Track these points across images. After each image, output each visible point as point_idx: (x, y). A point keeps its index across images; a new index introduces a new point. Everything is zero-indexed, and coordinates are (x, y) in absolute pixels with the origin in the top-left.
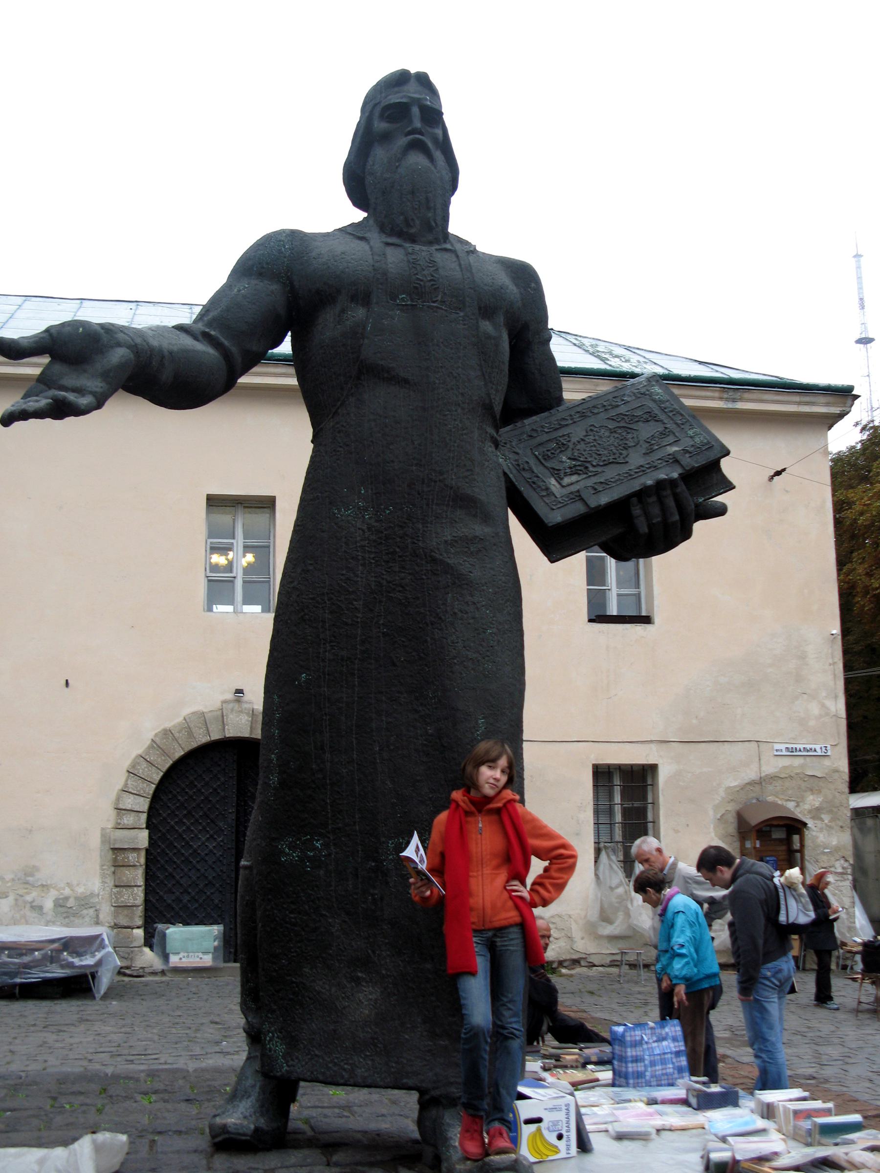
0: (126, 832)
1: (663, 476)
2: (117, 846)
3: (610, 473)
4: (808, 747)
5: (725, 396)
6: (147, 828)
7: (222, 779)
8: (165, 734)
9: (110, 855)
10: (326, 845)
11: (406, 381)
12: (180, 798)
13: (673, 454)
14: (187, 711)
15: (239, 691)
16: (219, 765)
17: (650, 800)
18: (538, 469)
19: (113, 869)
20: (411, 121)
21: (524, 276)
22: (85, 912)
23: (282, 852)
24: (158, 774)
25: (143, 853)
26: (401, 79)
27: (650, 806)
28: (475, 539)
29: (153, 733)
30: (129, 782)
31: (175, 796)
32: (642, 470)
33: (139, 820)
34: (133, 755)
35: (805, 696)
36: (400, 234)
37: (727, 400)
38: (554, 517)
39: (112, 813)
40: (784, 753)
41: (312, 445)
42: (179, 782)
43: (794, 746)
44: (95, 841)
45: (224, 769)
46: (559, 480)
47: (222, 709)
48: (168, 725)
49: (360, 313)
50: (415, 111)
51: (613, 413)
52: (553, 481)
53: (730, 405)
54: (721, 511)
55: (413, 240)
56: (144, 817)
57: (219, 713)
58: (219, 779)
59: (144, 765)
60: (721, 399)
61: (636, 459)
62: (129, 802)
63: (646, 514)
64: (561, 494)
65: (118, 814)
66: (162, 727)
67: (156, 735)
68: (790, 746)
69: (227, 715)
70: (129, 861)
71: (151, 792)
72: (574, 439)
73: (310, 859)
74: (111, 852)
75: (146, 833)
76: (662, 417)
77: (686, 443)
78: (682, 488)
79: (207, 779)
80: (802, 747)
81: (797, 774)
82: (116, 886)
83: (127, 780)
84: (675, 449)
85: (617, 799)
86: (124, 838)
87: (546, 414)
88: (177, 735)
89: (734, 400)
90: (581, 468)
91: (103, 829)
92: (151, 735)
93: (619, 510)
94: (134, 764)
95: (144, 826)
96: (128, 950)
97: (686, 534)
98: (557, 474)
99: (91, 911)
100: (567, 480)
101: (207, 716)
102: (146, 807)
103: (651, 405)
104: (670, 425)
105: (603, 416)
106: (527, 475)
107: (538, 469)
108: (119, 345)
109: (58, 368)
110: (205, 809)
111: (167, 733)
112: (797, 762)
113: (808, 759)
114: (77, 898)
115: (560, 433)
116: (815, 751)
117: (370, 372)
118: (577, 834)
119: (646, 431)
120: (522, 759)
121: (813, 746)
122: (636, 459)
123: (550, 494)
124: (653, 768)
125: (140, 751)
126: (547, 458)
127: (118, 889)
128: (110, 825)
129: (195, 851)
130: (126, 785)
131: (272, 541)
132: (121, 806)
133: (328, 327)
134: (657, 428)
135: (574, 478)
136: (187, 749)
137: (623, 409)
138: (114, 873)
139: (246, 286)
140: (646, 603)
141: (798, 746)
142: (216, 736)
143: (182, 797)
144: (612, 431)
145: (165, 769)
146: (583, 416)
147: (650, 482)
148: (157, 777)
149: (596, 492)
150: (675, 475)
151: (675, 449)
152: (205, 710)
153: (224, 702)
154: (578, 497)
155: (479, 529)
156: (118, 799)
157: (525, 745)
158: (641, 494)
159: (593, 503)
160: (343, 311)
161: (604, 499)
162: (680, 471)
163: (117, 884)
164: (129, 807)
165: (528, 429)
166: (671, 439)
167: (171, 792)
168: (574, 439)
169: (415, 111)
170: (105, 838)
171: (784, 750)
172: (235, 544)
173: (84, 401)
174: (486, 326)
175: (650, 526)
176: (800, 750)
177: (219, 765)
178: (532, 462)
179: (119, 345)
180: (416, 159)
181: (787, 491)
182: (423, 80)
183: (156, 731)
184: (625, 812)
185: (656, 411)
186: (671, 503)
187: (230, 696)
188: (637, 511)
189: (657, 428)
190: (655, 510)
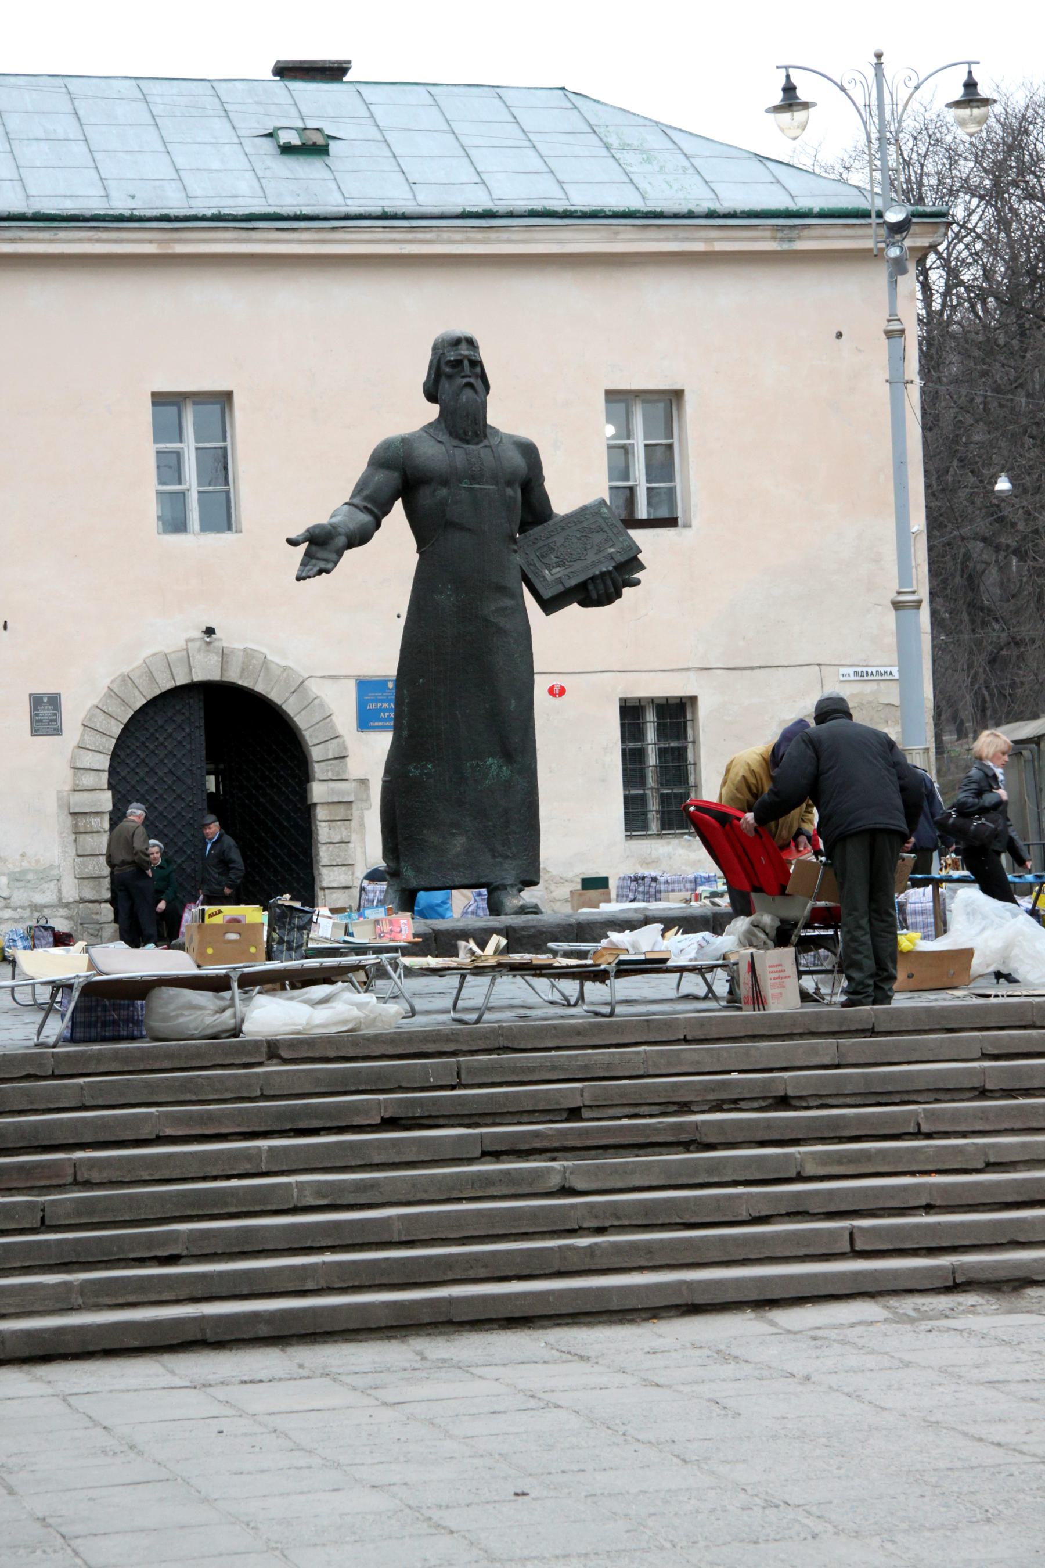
0: (85, 795)
1: (604, 569)
2: (77, 810)
3: (577, 566)
4: (882, 670)
5: (780, 235)
6: (109, 789)
7: (188, 730)
8: (124, 681)
9: (69, 821)
10: (434, 766)
11: (470, 530)
12: (139, 753)
13: (611, 554)
14: (147, 652)
15: (210, 631)
16: (183, 714)
17: (690, 738)
18: (538, 564)
19: (74, 836)
20: (463, 369)
21: (529, 451)
22: (46, 886)
23: (410, 771)
24: (118, 726)
25: (107, 818)
26: (457, 342)
27: (690, 746)
28: (506, 608)
29: (109, 680)
30: (86, 737)
31: (134, 751)
32: (594, 564)
33: (100, 779)
34: (88, 706)
35: (880, 608)
36: (461, 439)
37: (782, 239)
38: (547, 594)
39: (70, 773)
40: (852, 678)
41: (418, 556)
42: (137, 734)
43: (865, 669)
44: (51, 806)
45: (189, 719)
46: (550, 571)
47: (187, 649)
48: (125, 670)
49: (444, 492)
50: (466, 362)
51: (579, 527)
52: (547, 572)
53: (786, 246)
54: (637, 583)
55: (468, 442)
56: (106, 775)
57: (185, 653)
58: (183, 729)
59: (102, 716)
60: (774, 238)
61: (591, 557)
62: (90, 760)
63: (596, 588)
64: (552, 577)
65: (75, 775)
66: (118, 673)
67: (112, 682)
68: (859, 669)
69: (193, 656)
70: (91, 826)
71: (112, 748)
72: (558, 544)
73: (426, 774)
74: (70, 817)
75: (109, 794)
76: (606, 529)
77: (619, 546)
78: (615, 574)
79: (170, 730)
80: (874, 670)
81: (870, 703)
82: (79, 856)
83: (82, 735)
84: (612, 550)
85: (651, 735)
86: (83, 801)
87: (540, 527)
88: (136, 681)
89: (791, 240)
90: (561, 564)
91: (59, 792)
92: (106, 682)
93: (583, 586)
94: (90, 716)
95: (106, 786)
96: (98, 926)
97: (619, 595)
98: (548, 567)
99: (52, 885)
100: (554, 571)
101: (172, 658)
102: (106, 765)
103: (601, 520)
104: (611, 534)
105: (574, 528)
106: (532, 568)
107: (538, 564)
108: (340, 534)
109: (314, 548)
110: (170, 766)
111: (126, 679)
112: (869, 688)
113: (882, 684)
114: (36, 872)
115: (551, 540)
116: (891, 673)
117: (450, 525)
118: (603, 781)
119: (597, 538)
120: (534, 741)
121: (888, 669)
122: (591, 557)
123: (545, 579)
124: (693, 699)
125: (95, 702)
126: (543, 556)
127: (81, 859)
128: (68, 787)
129: (161, 814)
130: (82, 739)
131: (228, 443)
132: (79, 765)
133: (426, 497)
134: (605, 536)
135: (558, 569)
136: (149, 697)
137: (585, 524)
138: (75, 841)
139: (380, 476)
140: (682, 500)
141: (869, 670)
142: (182, 680)
143: (143, 752)
144: (579, 539)
145: (125, 721)
146: (563, 529)
147: (597, 573)
148: (117, 730)
149: (570, 578)
150: (611, 568)
151: (612, 550)
152: (167, 651)
153: (188, 641)
154: (559, 581)
155: (508, 602)
156: (73, 758)
157: (536, 677)
158: (593, 579)
159: (568, 586)
160: (435, 490)
161: (573, 582)
162: (614, 564)
163: (80, 853)
164: (88, 766)
165: (532, 538)
166: (611, 543)
167: (129, 747)
168: (558, 544)
169: (466, 362)
170: (63, 803)
171: (852, 674)
172: (186, 449)
173: (330, 566)
174: (509, 491)
175: (598, 595)
176: (872, 674)
177: (183, 714)
178: (536, 560)
179: (340, 534)
180: (468, 393)
181: (860, 351)
182: (471, 342)
183: (113, 678)
184: (662, 753)
185: (604, 525)
186: (609, 582)
187: (198, 634)
188: (591, 587)
189: (605, 536)
190: (601, 587)
